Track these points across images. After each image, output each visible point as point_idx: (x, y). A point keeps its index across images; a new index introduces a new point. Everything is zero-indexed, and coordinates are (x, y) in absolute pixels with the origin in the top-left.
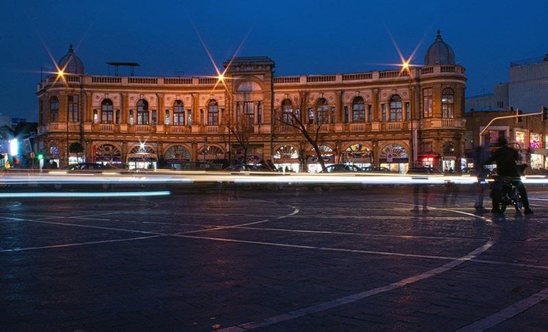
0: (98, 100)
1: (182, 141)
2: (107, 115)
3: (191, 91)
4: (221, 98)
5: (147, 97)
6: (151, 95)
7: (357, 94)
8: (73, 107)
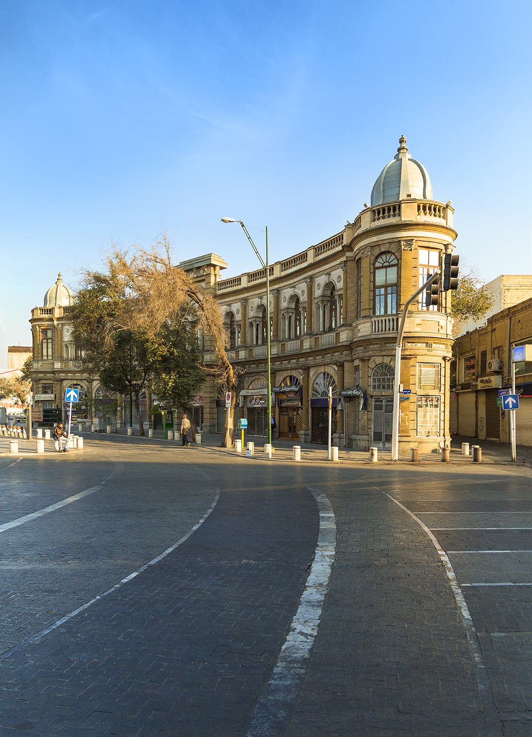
0: (68, 334)
8: (47, 343)
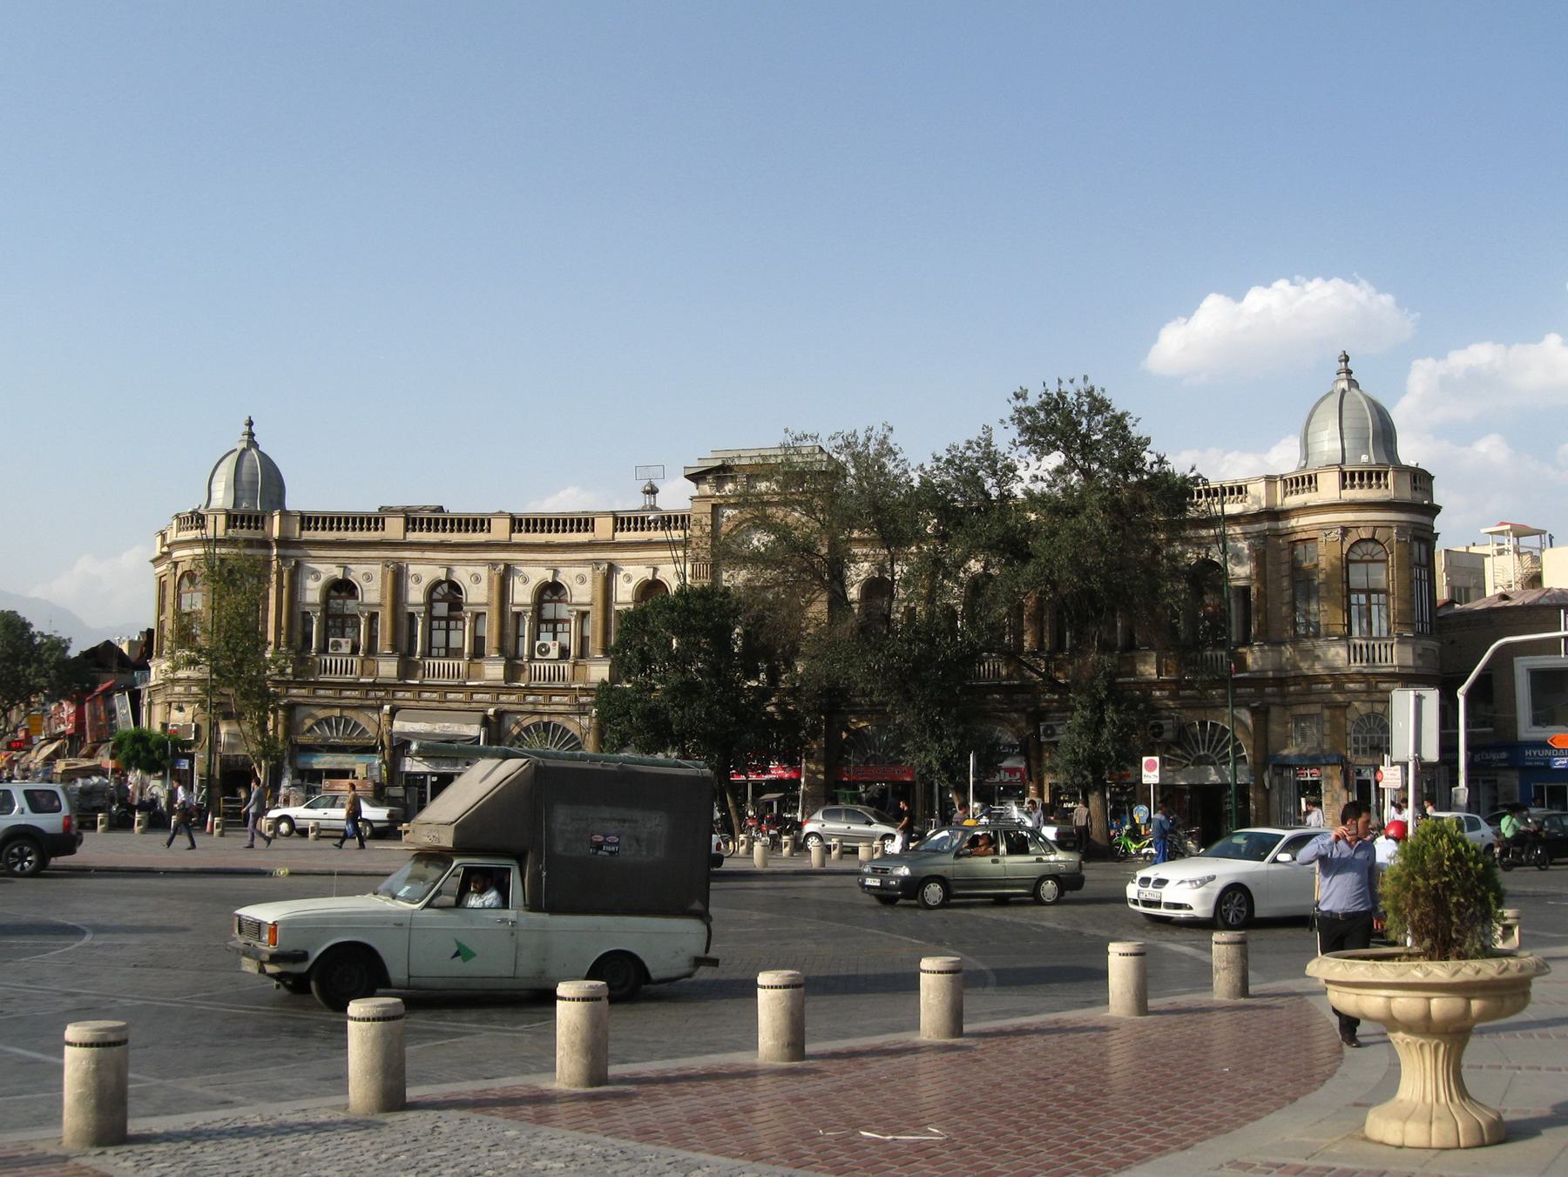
1: (561, 708)
2: (448, 630)
3: (589, 555)
4: (369, 578)
5: (462, 575)
6: (471, 569)
7: (338, 573)
